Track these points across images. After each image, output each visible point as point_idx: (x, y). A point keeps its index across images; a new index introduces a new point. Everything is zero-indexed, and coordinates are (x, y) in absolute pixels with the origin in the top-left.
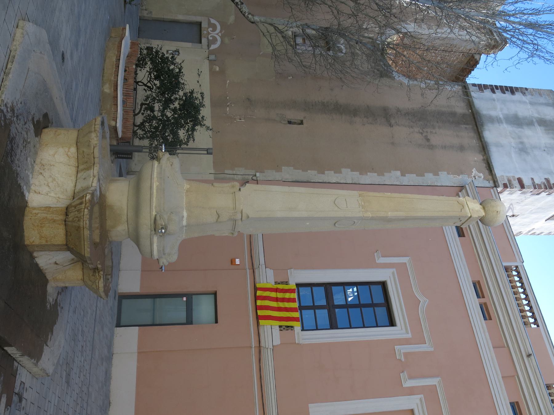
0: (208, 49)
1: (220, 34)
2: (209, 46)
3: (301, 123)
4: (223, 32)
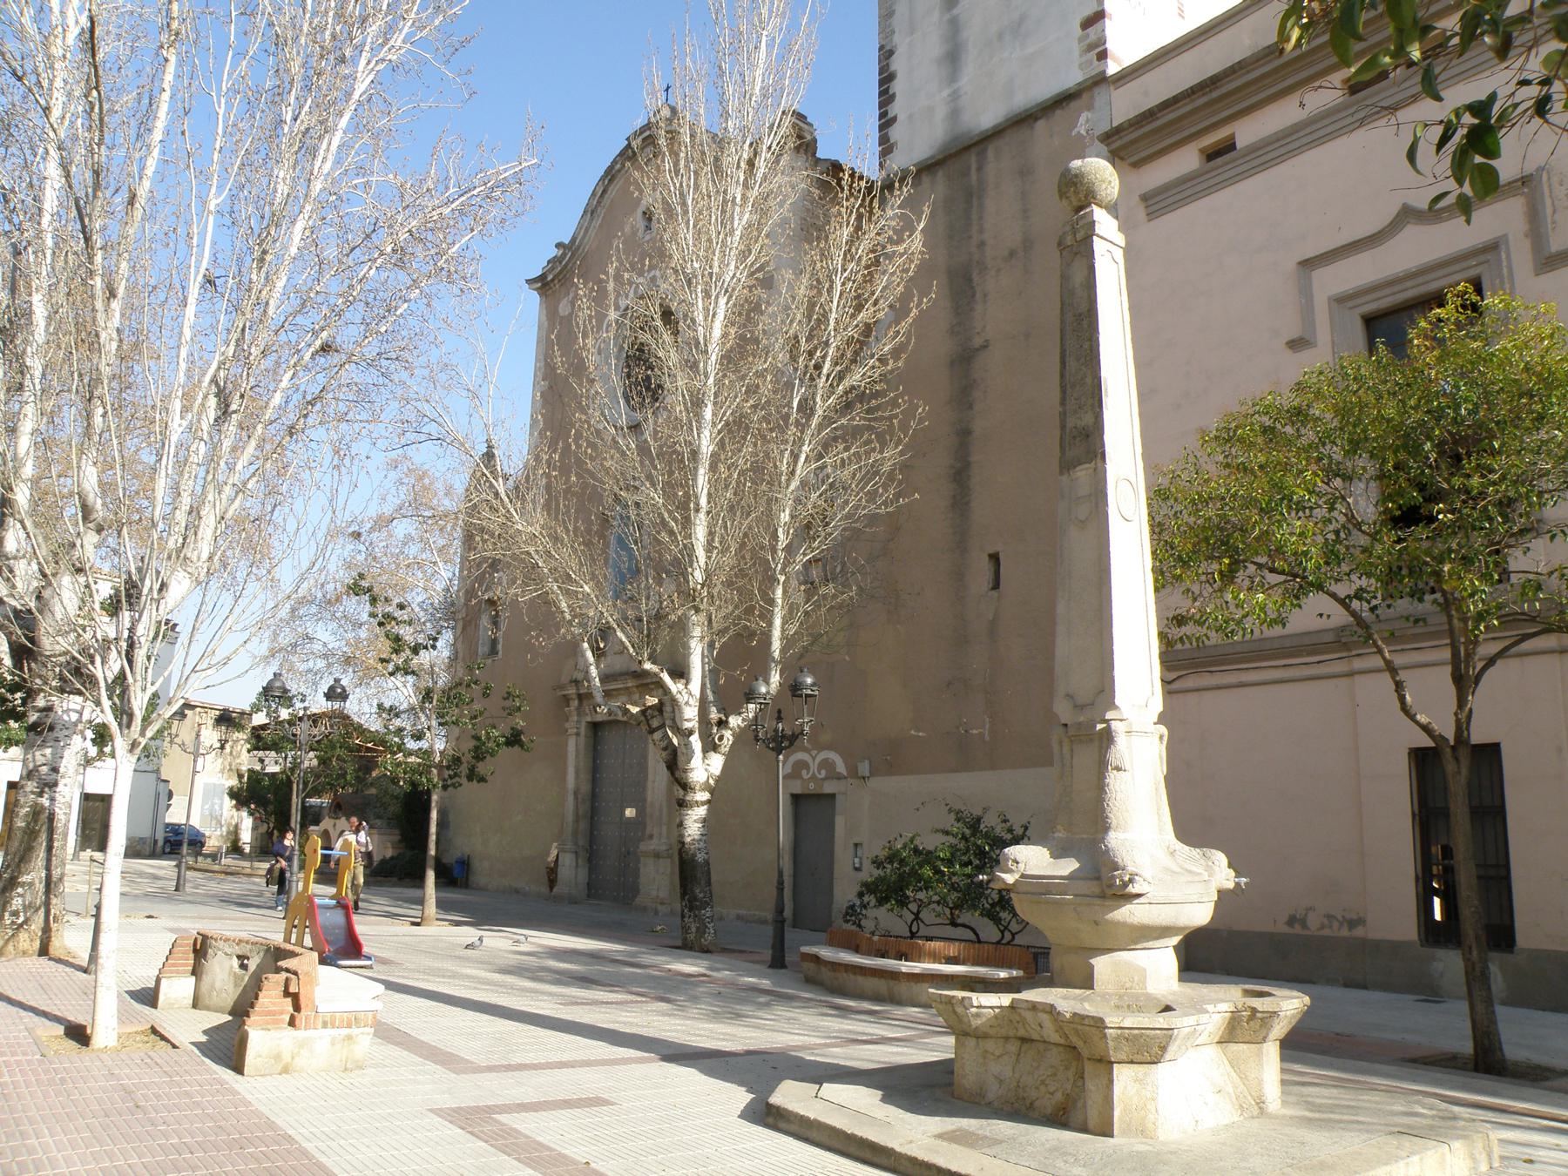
1: (814, 753)
2: (839, 777)
3: (995, 558)
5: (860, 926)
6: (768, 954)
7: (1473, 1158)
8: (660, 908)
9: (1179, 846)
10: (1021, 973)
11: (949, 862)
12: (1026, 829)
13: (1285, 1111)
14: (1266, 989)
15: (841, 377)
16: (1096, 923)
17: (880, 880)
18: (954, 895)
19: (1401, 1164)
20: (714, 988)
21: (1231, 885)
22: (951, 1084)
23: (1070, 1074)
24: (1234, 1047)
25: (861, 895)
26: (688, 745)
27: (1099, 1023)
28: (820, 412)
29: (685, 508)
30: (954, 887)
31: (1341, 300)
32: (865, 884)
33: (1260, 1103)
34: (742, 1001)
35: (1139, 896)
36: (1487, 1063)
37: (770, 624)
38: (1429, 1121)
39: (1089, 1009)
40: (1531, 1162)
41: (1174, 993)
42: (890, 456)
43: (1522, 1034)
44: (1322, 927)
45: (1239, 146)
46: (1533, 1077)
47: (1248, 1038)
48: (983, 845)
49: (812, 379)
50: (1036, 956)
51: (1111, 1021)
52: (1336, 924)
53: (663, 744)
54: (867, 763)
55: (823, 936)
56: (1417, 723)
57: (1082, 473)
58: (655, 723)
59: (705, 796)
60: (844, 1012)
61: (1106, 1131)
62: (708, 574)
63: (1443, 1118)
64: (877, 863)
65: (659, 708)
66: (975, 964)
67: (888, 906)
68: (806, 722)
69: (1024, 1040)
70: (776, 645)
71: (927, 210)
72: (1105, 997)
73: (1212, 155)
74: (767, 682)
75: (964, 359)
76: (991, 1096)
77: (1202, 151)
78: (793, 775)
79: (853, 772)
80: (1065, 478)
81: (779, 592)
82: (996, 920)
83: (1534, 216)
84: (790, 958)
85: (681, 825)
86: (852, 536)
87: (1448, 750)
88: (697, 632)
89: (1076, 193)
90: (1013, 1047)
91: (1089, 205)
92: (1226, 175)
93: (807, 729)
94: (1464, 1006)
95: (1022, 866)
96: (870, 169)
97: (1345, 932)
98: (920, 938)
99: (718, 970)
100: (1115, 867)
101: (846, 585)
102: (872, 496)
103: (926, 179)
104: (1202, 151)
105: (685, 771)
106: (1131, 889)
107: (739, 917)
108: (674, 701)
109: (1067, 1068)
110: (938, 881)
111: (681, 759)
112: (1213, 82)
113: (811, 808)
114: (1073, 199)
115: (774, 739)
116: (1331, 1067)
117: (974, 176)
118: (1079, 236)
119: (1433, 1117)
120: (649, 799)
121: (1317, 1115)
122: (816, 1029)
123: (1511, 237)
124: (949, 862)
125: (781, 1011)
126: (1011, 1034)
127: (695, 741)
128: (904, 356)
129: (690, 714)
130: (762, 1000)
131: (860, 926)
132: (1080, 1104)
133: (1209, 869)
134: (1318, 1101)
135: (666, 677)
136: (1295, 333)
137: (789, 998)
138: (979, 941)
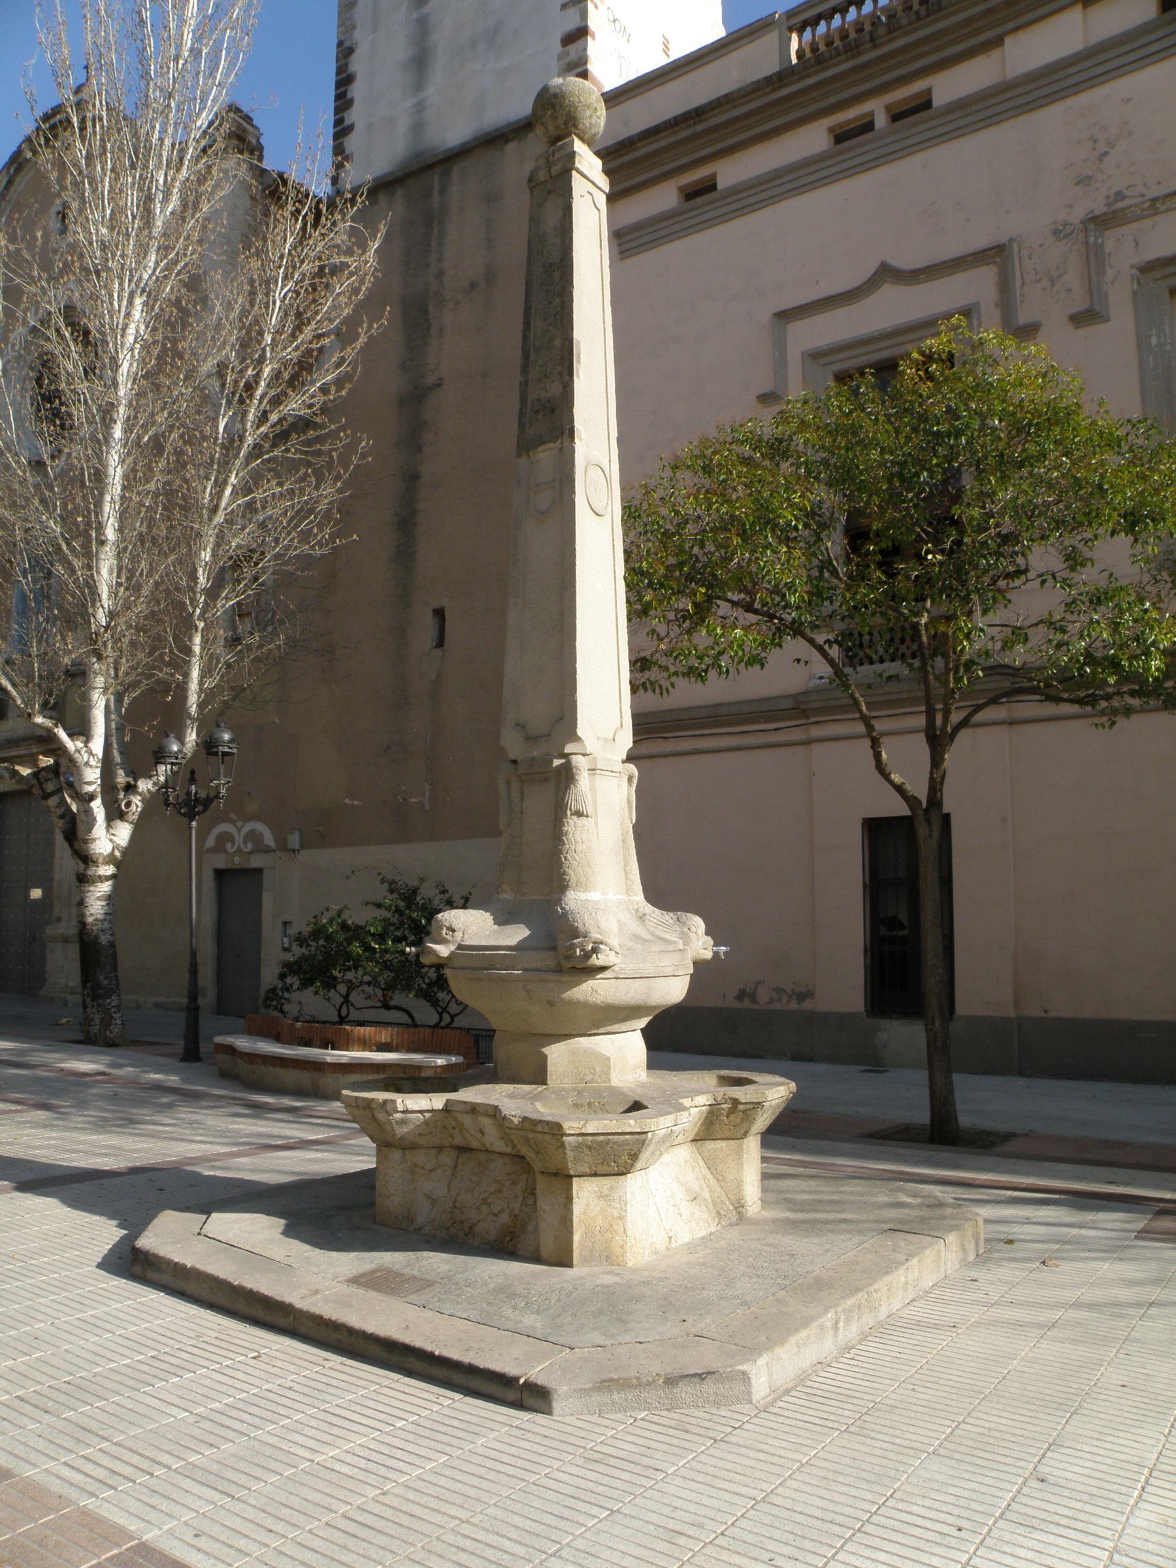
0: (273, 851)
1: (239, 824)
2: (268, 850)
3: (439, 614)
4: (232, 816)
5: (282, 1011)
6: (180, 1046)
7: (964, 1249)
8: (69, 998)
9: (649, 908)
10: (460, 1059)
11: (381, 938)
13: (769, 1214)
14: (744, 1074)
15: (276, 401)
16: (551, 1004)
17: (304, 958)
18: (388, 975)
19: (902, 1270)
20: (109, 1088)
21: (708, 955)
22: (372, 1204)
24: (711, 1145)
25: (282, 976)
26: (89, 812)
27: (555, 1130)
28: (250, 440)
29: (87, 536)
30: (386, 966)
31: (815, 356)
32: (287, 965)
33: (739, 1206)
34: (141, 1103)
35: (603, 969)
36: (943, 1134)
37: (187, 675)
38: (915, 1213)
39: (543, 1110)
40: (1011, 1242)
41: (643, 1085)
42: (329, 492)
43: (980, 1099)
44: (771, 1001)
45: (719, 187)
46: (983, 1144)
47: (727, 1134)
48: (415, 916)
49: (241, 401)
50: (477, 1039)
51: (571, 1126)
52: (785, 998)
53: (60, 811)
54: (297, 834)
55: (241, 1023)
56: (891, 782)
57: (545, 455)
58: (50, 787)
59: (109, 870)
60: (259, 1110)
61: (564, 1260)
62: (112, 615)
63: (929, 1206)
64: (301, 940)
65: (55, 770)
66: (410, 1050)
67: (311, 989)
68: (222, 784)
69: (462, 1150)
70: (193, 700)
71: (383, 229)
72: (560, 1093)
73: (691, 194)
74: (181, 740)
75: (415, 398)
78: (219, 848)
79: (282, 844)
80: (523, 461)
81: (197, 640)
82: (434, 1002)
83: (1005, 285)
84: (204, 1048)
85: (81, 903)
86: (284, 580)
87: (921, 812)
88: (99, 681)
89: (554, 117)
90: (447, 1158)
91: (569, 134)
93: (223, 791)
94: (922, 1076)
95: (458, 935)
96: (320, 188)
97: (794, 1006)
98: (348, 1023)
99: (120, 1066)
100: (575, 933)
101: (275, 634)
102: (305, 536)
103: (382, 197)
104: (681, 189)
105: (86, 842)
106: (596, 961)
107: (157, 1005)
108: (72, 761)
109: (514, 1183)
110: (369, 959)
111: (81, 827)
112: (698, 114)
113: (236, 885)
114: (551, 127)
115: (186, 804)
116: (793, 1149)
117: (436, 198)
118: (556, 170)
119: (920, 1205)
120: (57, 878)
121: (801, 1216)
122: (223, 1134)
123: (982, 305)
124: (381, 938)
125: (186, 1113)
126: (445, 1143)
127: (97, 806)
128: (348, 386)
129: (92, 776)
130: (164, 1100)
131: (282, 1011)
132: (530, 1228)
133: (684, 937)
134: (799, 1197)
135: (62, 734)
136: (766, 388)
137: (196, 1096)
138: (416, 1026)
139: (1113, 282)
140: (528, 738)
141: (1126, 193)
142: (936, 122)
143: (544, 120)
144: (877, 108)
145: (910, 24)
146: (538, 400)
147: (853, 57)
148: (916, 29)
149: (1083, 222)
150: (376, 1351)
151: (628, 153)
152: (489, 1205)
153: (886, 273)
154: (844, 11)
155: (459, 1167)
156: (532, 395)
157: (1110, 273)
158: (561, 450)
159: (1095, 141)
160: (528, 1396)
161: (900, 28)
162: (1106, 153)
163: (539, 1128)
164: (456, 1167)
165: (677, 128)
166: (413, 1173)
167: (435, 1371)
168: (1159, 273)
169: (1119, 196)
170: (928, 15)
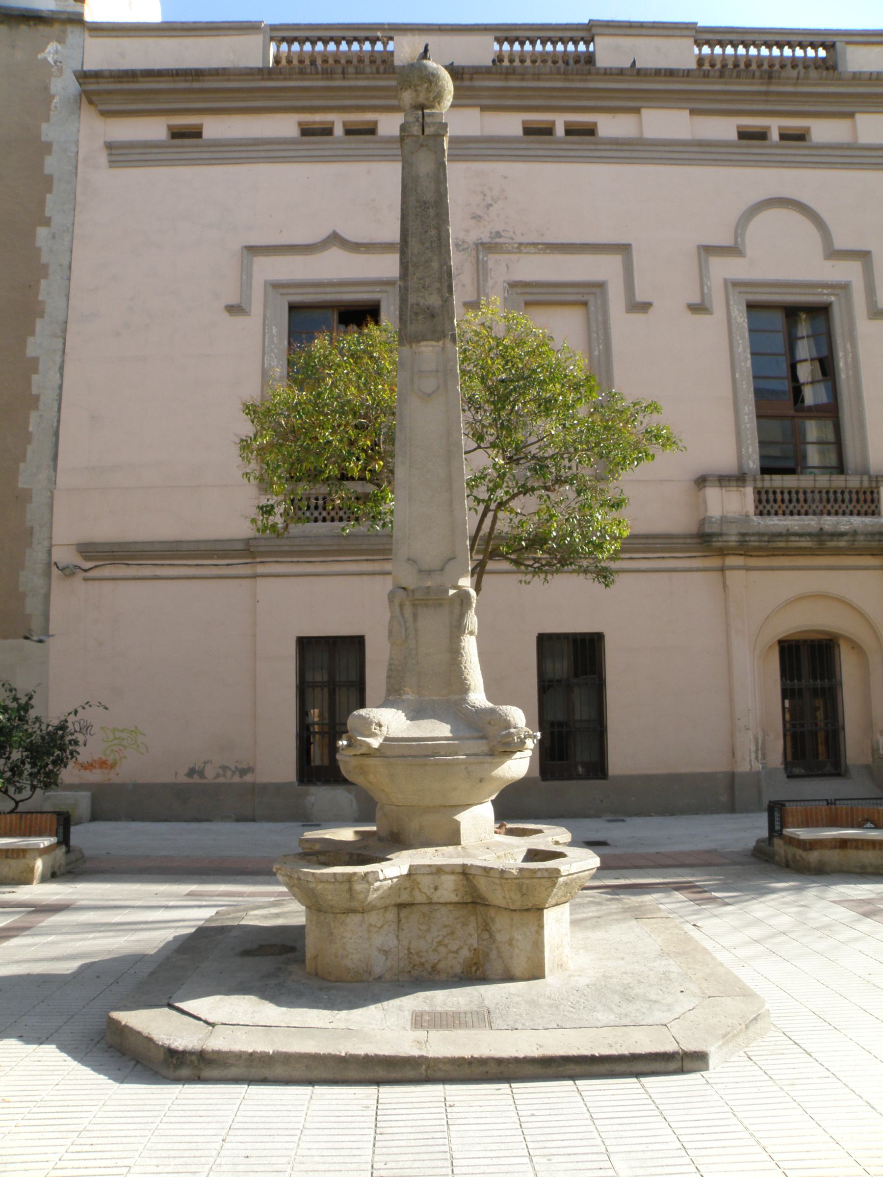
12: (31, 698)
23: (471, 928)
31: (276, 286)
44: (218, 776)
52: (229, 773)
61: (536, 973)
73: (177, 134)
76: (378, 970)
77: (524, 122)
89: (428, 90)
92: (190, 156)
95: (384, 729)
97: (237, 779)
109: (465, 924)
112: (198, 74)
136: (234, 300)
139: (492, 288)
140: (420, 571)
141: (503, 234)
142: (378, 146)
143: (419, 88)
144: (338, 121)
145: (371, 73)
146: (417, 304)
147: (327, 79)
148: (374, 79)
149: (476, 245)
150: (539, 1070)
151: (128, 82)
152: (446, 946)
153: (335, 239)
154: (326, 43)
155: (403, 921)
156: (412, 299)
157: (490, 283)
158: (443, 348)
159: (485, 195)
160: (684, 1062)
161: (364, 73)
162: (491, 205)
163: (539, 875)
164: (399, 921)
165: (177, 79)
166: (369, 932)
167: (595, 1069)
168: (519, 290)
169: (498, 234)
170: (385, 73)
